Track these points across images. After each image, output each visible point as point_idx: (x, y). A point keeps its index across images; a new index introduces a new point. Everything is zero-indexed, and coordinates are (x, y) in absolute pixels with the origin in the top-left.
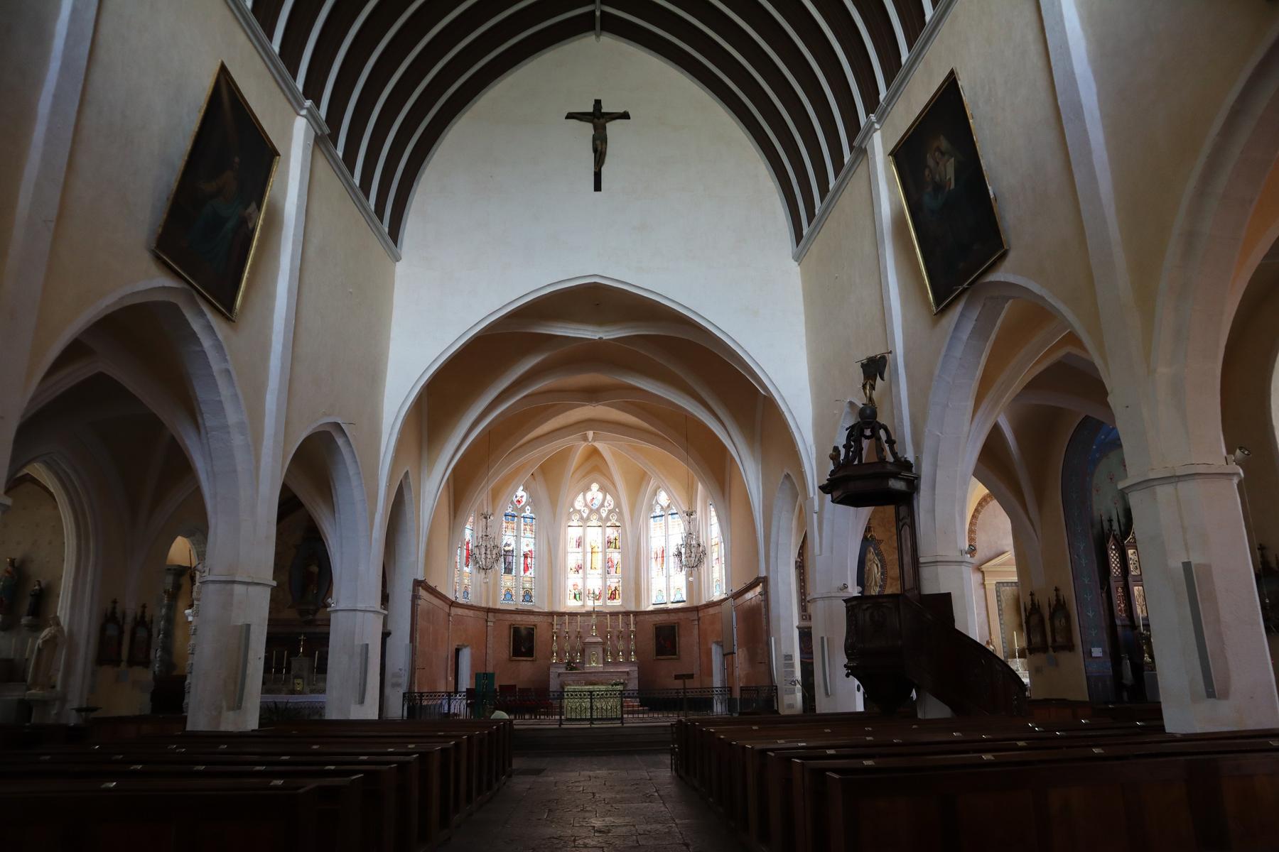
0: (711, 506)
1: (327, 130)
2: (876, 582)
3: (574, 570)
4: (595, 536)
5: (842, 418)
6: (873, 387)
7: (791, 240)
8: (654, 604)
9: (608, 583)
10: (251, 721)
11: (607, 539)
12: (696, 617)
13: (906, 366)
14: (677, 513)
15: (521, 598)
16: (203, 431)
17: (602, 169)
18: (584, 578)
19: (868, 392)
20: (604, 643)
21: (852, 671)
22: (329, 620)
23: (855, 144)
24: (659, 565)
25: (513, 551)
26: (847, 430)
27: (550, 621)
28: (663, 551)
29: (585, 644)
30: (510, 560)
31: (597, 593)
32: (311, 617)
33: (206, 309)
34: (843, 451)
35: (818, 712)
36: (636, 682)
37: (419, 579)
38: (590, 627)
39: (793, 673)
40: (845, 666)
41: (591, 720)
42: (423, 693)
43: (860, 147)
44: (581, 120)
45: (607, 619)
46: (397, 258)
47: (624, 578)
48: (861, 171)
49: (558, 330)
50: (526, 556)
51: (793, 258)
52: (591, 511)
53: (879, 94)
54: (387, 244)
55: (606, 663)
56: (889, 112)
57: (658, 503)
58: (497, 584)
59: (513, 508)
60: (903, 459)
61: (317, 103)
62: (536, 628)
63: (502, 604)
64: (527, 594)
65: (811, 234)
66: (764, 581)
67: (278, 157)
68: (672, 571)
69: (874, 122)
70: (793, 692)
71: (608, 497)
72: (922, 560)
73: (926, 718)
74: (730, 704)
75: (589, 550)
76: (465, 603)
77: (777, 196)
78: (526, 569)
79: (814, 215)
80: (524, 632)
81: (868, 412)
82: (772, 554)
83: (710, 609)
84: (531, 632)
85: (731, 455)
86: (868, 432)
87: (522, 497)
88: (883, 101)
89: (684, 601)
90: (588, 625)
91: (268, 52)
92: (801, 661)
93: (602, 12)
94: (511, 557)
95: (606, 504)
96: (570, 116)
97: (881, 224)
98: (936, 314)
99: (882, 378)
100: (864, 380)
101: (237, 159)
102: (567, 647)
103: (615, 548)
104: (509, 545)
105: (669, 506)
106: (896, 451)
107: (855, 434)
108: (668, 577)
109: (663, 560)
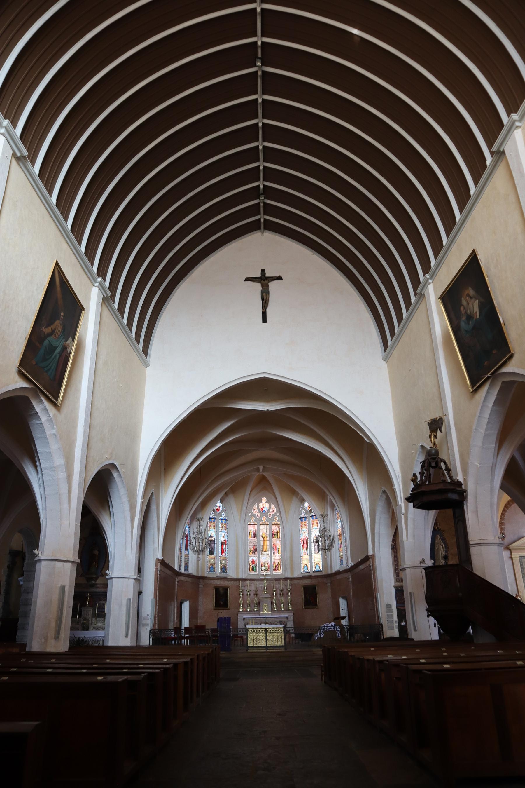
1: (109, 294)
3: (252, 552)
4: (263, 530)
6: (435, 437)
8: (302, 573)
9: (273, 560)
16: (39, 470)
17: (267, 310)
18: (259, 558)
23: (418, 291)
24: (305, 548)
25: (214, 540)
26: (421, 463)
27: (238, 584)
28: (307, 539)
32: (93, 582)
33: (43, 398)
34: (419, 476)
38: (263, 588)
43: (421, 293)
44: (253, 281)
45: (273, 583)
47: (283, 556)
48: (422, 307)
49: (243, 406)
53: (430, 263)
55: (273, 611)
56: (437, 273)
60: (456, 480)
61: (104, 279)
62: (230, 589)
65: (393, 345)
66: (373, 556)
67: (84, 311)
68: (313, 552)
69: (428, 279)
71: (273, 506)
75: (261, 539)
77: (372, 322)
82: (376, 540)
84: (226, 589)
86: (433, 464)
87: (219, 507)
88: (433, 266)
89: (321, 571)
91: (78, 252)
95: (271, 510)
96: (247, 279)
99: (441, 431)
100: (430, 432)
101: (62, 314)
102: (248, 601)
108: (311, 555)
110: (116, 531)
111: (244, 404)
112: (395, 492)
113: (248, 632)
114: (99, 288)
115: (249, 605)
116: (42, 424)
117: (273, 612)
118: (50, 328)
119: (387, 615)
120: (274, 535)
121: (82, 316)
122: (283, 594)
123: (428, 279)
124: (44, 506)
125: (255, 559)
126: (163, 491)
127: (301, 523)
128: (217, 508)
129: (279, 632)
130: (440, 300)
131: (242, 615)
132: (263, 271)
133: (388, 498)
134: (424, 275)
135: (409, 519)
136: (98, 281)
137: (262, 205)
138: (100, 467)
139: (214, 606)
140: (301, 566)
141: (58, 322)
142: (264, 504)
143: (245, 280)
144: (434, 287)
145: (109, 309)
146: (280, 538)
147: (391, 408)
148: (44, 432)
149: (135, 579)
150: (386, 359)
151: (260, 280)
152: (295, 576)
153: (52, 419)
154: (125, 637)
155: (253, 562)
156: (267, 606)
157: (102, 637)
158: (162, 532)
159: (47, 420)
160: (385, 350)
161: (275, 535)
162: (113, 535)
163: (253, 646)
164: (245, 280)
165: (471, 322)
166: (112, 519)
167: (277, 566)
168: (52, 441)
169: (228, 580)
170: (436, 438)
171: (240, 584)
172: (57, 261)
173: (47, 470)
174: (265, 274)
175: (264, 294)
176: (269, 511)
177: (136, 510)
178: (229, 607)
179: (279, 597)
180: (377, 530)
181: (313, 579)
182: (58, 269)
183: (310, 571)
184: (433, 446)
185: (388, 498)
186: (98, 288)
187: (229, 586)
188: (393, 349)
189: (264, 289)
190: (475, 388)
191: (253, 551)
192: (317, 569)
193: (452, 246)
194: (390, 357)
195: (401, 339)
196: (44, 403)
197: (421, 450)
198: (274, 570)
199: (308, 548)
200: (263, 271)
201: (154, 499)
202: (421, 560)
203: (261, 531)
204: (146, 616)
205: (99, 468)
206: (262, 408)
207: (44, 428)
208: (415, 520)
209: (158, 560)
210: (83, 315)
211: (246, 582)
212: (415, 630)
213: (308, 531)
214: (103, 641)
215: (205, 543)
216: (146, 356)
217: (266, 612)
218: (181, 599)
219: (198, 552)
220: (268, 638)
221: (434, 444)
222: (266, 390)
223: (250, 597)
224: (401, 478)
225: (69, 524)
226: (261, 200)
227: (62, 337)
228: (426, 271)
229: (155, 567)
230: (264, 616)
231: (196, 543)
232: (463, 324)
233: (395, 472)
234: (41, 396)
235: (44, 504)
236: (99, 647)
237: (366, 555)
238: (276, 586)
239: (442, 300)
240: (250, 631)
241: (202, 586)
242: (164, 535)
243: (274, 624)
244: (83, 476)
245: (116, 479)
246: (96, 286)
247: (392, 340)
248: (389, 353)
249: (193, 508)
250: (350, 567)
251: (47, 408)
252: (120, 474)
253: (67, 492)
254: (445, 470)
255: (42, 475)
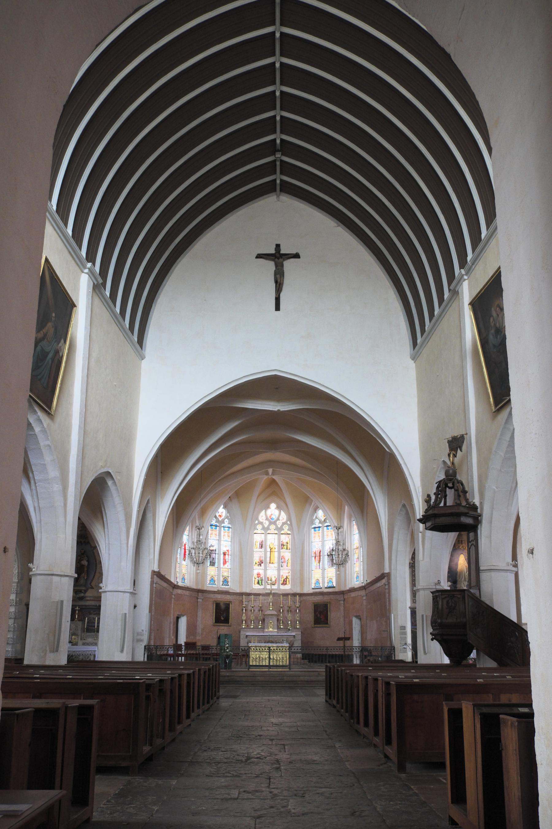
0: (354, 522)
1: (100, 281)
2: (465, 578)
3: (258, 564)
4: (272, 540)
5: (439, 471)
6: (455, 456)
7: (410, 345)
8: (313, 589)
9: (281, 574)
10: (63, 661)
11: (281, 543)
12: (342, 599)
13: (477, 442)
14: (330, 526)
15: (221, 583)
16: (32, 482)
17: (281, 295)
18: (265, 570)
19: (451, 459)
20: (278, 615)
21: (435, 637)
22: (101, 597)
23: (451, 288)
24: (317, 562)
25: (216, 550)
26: (436, 483)
27: (241, 599)
28: (320, 551)
29: (264, 615)
30: (214, 557)
31: (274, 579)
32: (82, 595)
33: (37, 409)
34: (433, 498)
35: (419, 662)
36: (300, 642)
37: (155, 570)
38: (268, 604)
39: (406, 638)
40: (431, 634)
41: (269, 666)
42: (158, 646)
43: (454, 289)
44: (266, 259)
45: (280, 598)
46: (142, 358)
47: (293, 570)
48: (455, 305)
49: (251, 405)
50: (224, 554)
51: (410, 358)
52: (271, 523)
53: (467, 256)
54: (136, 349)
55: (279, 628)
56: (474, 269)
57: (317, 518)
58: (204, 574)
59: (216, 520)
60: (472, 503)
61: (94, 264)
62: (231, 604)
63: (208, 586)
64: (225, 580)
65: (423, 343)
66: (388, 575)
67: (75, 308)
68: (326, 566)
69: (463, 275)
70: (406, 652)
71: (282, 513)
72: (481, 568)
73: (484, 667)
74: (362, 657)
75: (269, 550)
76: (183, 586)
77: (401, 314)
78: (225, 562)
79: (434, 315)
80: (223, 607)
81: (451, 471)
82: (393, 557)
83: (352, 593)
84: (227, 606)
85: (368, 491)
86: (450, 485)
87: (222, 513)
88: (470, 261)
89: (334, 587)
90: (267, 602)
91: (64, 235)
92: (412, 631)
93: (281, 180)
94: (214, 554)
95: (281, 518)
96: (259, 256)
97: (465, 346)
98: (494, 412)
99: (461, 450)
100: (450, 451)
101: (54, 315)
102: (252, 617)
103: (287, 549)
104: (213, 546)
105: (325, 520)
106: (468, 497)
107: (442, 487)
108: (324, 569)
109: (320, 558)
110: (110, 543)
111: (252, 403)
112: (414, 507)
113: (250, 650)
114: (89, 275)
115: (253, 622)
116: (36, 434)
117: (279, 630)
118: (42, 332)
119: (401, 637)
120: (283, 546)
121: (74, 314)
122: (291, 611)
123: (463, 275)
124: (38, 519)
125: (262, 572)
126: (160, 498)
127: (314, 533)
128: (219, 514)
129: (283, 651)
130: (470, 306)
131: (244, 633)
132: (278, 246)
133: (407, 513)
134: (460, 270)
135: (426, 538)
136: (87, 267)
137: (278, 163)
138: (95, 476)
139: (214, 622)
140: (312, 581)
141: (50, 325)
142: (273, 510)
143: (257, 257)
144: (469, 284)
145: (99, 298)
146: (289, 549)
147: (416, 415)
148: (38, 443)
149: (131, 593)
150: (414, 358)
151: (274, 258)
152: (307, 590)
153: (46, 430)
154: (120, 652)
155: (258, 575)
156: (273, 623)
157: (72, 652)
158: (159, 541)
159: (41, 431)
160: (414, 348)
161: (284, 545)
162: (107, 547)
163: (255, 664)
164: (257, 257)
165: (499, 337)
166: (106, 530)
167: (285, 580)
168: (45, 452)
169: (230, 594)
170: (456, 456)
171: (243, 599)
172: (46, 256)
173: (42, 482)
174: (280, 250)
175: (278, 276)
176: (278, 519)
177: (131, 520)
178: (231, 623)
179: (286, 613)
180: (394, 547)
181: (325, 596)
182: (47, 265)
183: (321, 586)
184: (451, 466)
185: (407, 513)
186: (88, 275)
187: (231, 600)
188: (422, 348)
189: (278, 269)
190: (498, 408)
191: (259, 563)
192: (330, 585)
193: (491, 241)
194: (418, 357)
195: (432, 337)
196: (37, 413)
197: (443, 466)
198: (282, 584)
199: (321, 561)
200: (278, 246)
201: (150, 506)
202: (436, 581)
203: (268, 541)
204: (140, 631)
205: (93, 478)
206: (273, 408)
207: (38, 439)
208: (433, 539)
209: (154, 572)
210: (74, 312)
211: (250, 597)
212: (425, 653)
213: (321, 542)
214: (95, 656)
215: (205, 555)
216: (141, 347)
217: (271, 630)
218: (178, 613)
219: (198, 564)
220: (271, 657)
221: (453, 463)
222: (277, 388)
223: (255, 613)
224: (421, 493)
225: (66, 538)
226: (277, 157)
227: (54, 340)
228: (462, 266)
229: (150, 580)
230: (268, 634)
231: (195, 553)
232: (491, 337)
233: (415, 487)
234: (35, 407)
235: (38, 517)
236: (90, 661)
237: (383, 572)
238: (283, 601)
239: (472, 307)
240: (253, 650)
241: (201, 601)
242: (160, 545)
243: (279, 643)
244: (79, 487)
245: (110, 488)
246: (85, 273)
247: (421, 337)
248: (418, 352)
249: (192, 514)
250: (365, 584)
251: (41, 418)
252: (115, 482)
253: (63, 505)
254: (462, 492)
255: (36, 487)
